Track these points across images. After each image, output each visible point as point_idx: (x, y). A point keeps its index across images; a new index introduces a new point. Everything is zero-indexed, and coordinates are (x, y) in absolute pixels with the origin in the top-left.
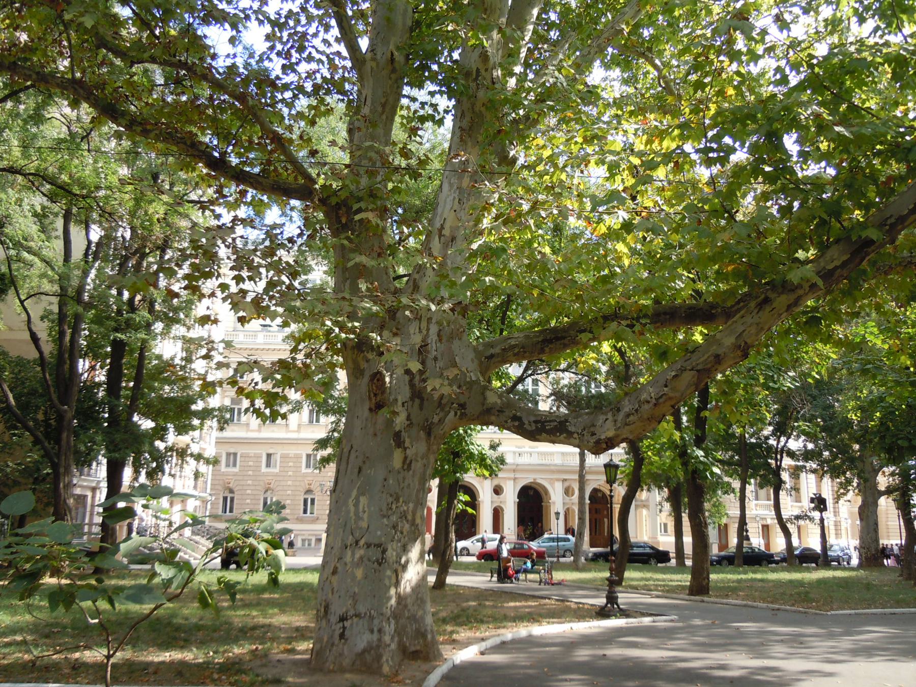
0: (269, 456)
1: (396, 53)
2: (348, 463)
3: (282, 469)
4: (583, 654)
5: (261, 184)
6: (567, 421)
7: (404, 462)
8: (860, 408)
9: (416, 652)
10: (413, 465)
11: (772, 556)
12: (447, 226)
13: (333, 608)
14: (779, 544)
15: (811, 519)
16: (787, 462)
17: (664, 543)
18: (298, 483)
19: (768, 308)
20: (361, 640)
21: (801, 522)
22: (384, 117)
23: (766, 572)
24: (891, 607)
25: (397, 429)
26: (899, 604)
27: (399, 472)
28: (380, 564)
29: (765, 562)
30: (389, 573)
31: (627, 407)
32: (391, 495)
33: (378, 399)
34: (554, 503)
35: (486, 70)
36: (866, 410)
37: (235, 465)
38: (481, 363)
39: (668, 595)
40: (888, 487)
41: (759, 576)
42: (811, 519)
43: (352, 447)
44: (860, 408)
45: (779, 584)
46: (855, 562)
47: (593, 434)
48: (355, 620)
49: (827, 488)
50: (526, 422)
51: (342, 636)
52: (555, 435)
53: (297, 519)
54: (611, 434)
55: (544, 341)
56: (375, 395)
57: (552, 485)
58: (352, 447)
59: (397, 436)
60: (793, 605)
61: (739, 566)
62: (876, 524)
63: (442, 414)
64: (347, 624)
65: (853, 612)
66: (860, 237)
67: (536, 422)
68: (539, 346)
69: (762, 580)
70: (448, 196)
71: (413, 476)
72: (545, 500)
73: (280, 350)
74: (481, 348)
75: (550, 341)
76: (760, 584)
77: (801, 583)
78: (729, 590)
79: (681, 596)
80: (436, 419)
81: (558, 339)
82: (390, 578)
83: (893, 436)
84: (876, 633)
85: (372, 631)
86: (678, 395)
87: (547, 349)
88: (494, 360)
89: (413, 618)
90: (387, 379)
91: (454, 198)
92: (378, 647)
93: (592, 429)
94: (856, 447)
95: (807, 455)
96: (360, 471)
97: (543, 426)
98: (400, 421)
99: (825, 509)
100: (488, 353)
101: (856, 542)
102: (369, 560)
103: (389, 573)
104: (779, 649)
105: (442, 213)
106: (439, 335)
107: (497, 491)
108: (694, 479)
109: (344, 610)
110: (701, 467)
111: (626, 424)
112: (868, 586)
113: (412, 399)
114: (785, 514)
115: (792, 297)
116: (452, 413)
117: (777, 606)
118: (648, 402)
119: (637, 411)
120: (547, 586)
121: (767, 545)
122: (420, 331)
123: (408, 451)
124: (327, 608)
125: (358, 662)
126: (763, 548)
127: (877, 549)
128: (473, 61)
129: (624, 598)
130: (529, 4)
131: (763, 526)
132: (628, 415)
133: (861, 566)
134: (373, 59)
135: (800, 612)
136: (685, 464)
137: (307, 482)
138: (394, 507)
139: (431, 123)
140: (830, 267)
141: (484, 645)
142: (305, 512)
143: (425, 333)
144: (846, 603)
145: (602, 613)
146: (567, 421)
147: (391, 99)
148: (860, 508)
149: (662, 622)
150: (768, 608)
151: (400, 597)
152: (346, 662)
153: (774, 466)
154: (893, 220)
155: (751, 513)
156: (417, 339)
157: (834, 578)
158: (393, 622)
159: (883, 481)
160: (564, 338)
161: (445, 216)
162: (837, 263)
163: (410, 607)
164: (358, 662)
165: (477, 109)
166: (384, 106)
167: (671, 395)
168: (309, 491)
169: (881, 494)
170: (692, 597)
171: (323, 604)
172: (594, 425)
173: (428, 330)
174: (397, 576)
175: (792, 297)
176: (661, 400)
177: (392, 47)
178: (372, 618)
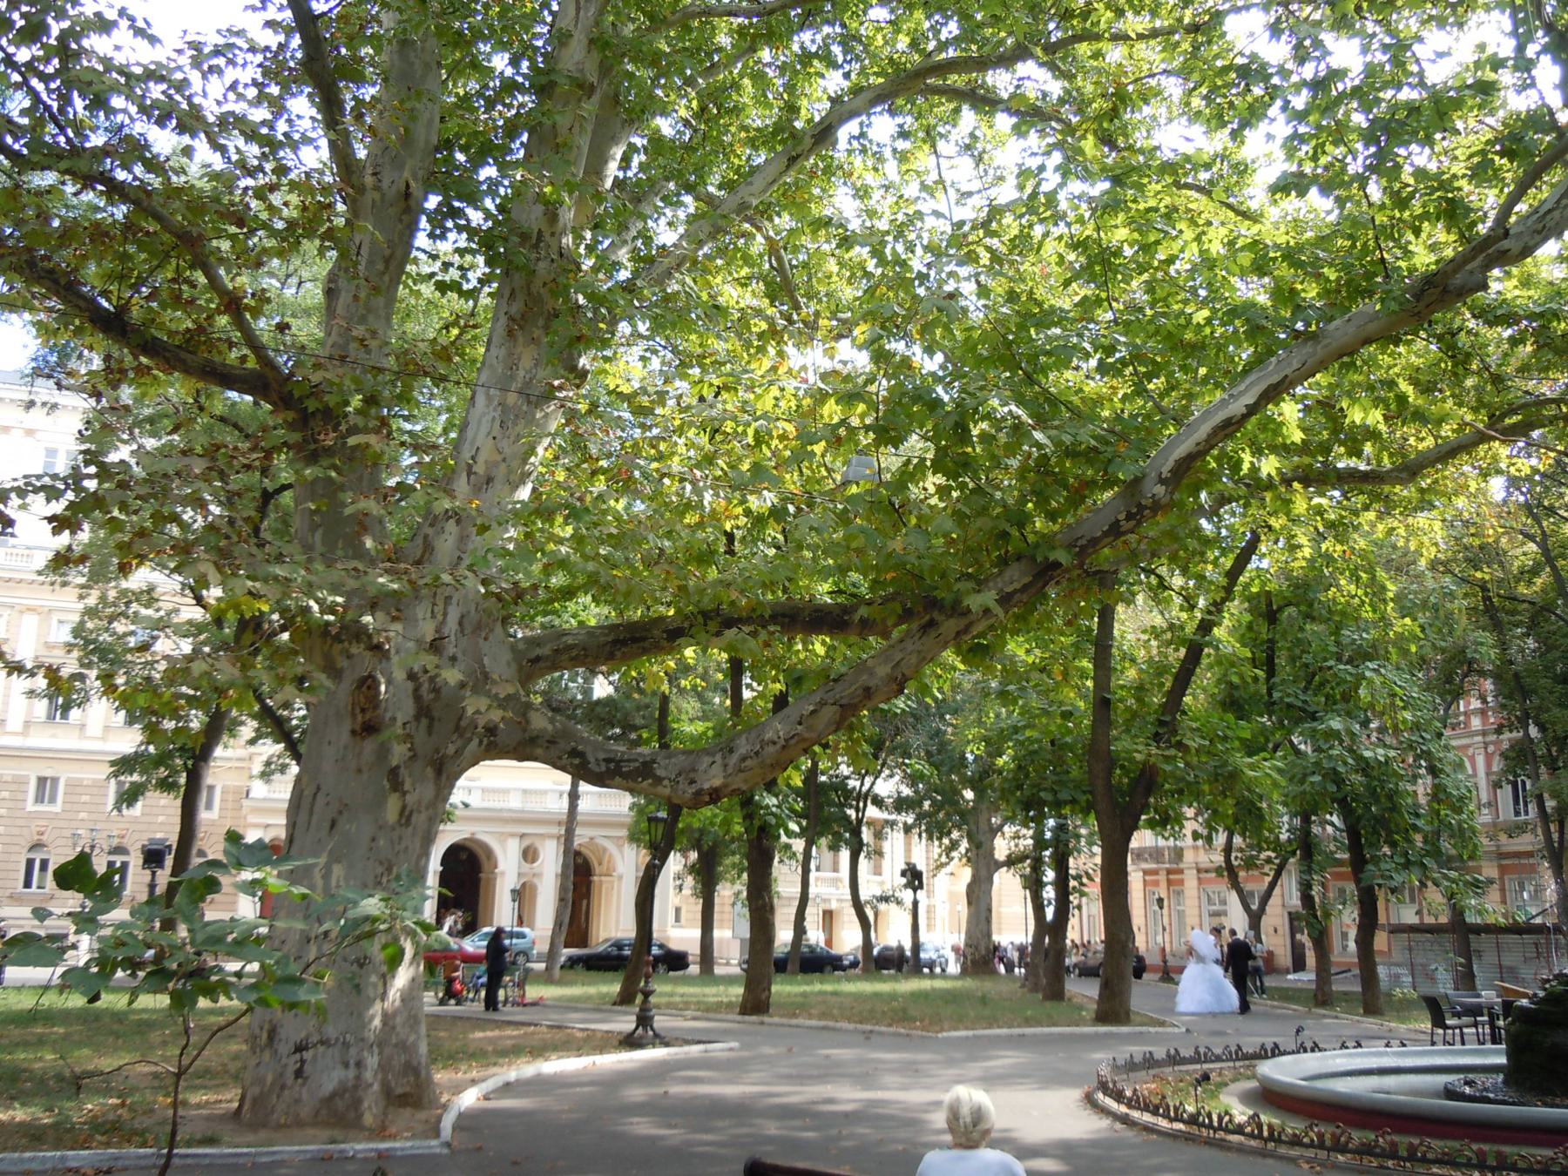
0: (42, 781)
1: (413, 184)
2: (311, 812)
3: (68, 807)
4: (637, 1094)
5: (184, 362)
6: (654, 761)
7: (401, 814)
8: (986, 740)
9: (405, 1095)
10: (414, 819)
11: (839, 958)
12: (481, 459)
13: (283, 1033)
14: (848, 940)
15: (899, 903)
16: (872, 812)
17: (682, 939)
18: (15, 831)
19: (933, 634)
20: (329, 1077)
21: (882, 907)
22: (386, 278)
23: (839, 980)
24: (1019, 1026)
25: (394, 763)
26: (1028, 1022)
27: (394, 829)
28: (361, 966)
29: (829, 968)
30: (374, 978)
31: (743, 747)
32: (381, 863)
33: (368, 717)
34: (503, 873)
35: (553, 234)
36: (994, 746)
37: (53, 800)
38: (520, 669)
39: (711, 1015)
40: (1009, 856)
41: (828, 987)
42: (899, 903)
43: (319, 789)
44: (986, 740)
45: (859, 997)
46: (954, 968)
47: (692, 782)
48: (321, 1049)
49: (923, 853)
50: (592, 760)
51: (299, 1073)
52: (635, 780)
53: (11, 897)
54: (717, 782)
55: (616, 642)
56: (363, 710)
57: (503, 842)
58: (319, 789)
59: (394, 773)
60: (890, 1025)
61: (793, 973)
62: (990, 911)
63: (459, 743)
64: (307, 1055)
65: (970, 1033)
66: (1047, 559)
67: (608, 761)
68: (608, 648)
69: (835, 994)
70: (484, 414)
71: (413, 835)
72: (485, 865)
73: (20, 581)
74: (521, 646)
75: (623, 643)
76: (833, 999)
77: (893, 996)
78: (799, 1007)
79: (730, 1017)
80: (451, 749)
81: (635, 640)
82: (375, 986)
83: (1033, 786)
84: (1007, 1059)
85: (346, 1065)
86: (813, 735)
87: (618, 654)
88: (542, 664)
89: (403, 1046)
90: (383, 688)
91: (494, 419)
92: (356, 1087)
93: (692, 775)
94: (969, 794)
95: (901, 804)
96: (333, 825)
97: (618, 767)
98: (399, 752)
99: (921, 886)
100: (533, 655)
101: (960, 939)
102: (345, 960)
103: (374, 978)
104: (890, 1079)
105: (474, 438)
106: (460, 624)
107: (529, 855)
108: (759, 838)
109: (303, 1035)
110: (773, 821)
111: (741, 771)
112: (984, 1000)
113: (417, 718)
114: (864, 895)
115: (963, 622)
116: (476, 741)
117: (869, 1027)
118: (774, 743)
119: (757, 753)
120: (516, 1009)
121: (829, 942)
122: (433, 616)
123: (408, 797)
124: (272, 1033)
125: (324, 1112)
126: (822, 944)
127: (987, 948)
128: (533, 217)
129: (660, 1022)
130: (613, 138)
131: (825, 912)
132: (744, 759)
133: (965, 971)
134: (377, 188)
135: (900, 1035)
136: (749, 817)
137: (35, 830)
138: (384, 880)
139: (455, 296)
140: (1009, 589)
141: (490, 1085)
142: (28, 884)
143: (440, 618)
144: (959, 1022)
145: (630, 1042)
146: (654, 761)
147: (399, 253)
148: (969, 886)
149: (718, 1049)
150: (856, 1031)
151: (386, 1017)
152: (305, 1112)
153: (854, 816)
154: (1084, 542)
155: (822, 894)
156: (428, 630)
157: (934, 990)
158: (376, 1049)
159: (1002, 847)
160: (644, 639)
161: (478, 444)
162: (1017, 586)
163: (398, 1029)
164: (324, 1112)
165: (534, 290)
166: (387, 261)
167: (806, 735)
168: (37, 846)
169: (999, 865)
170: (747, 1018)
171: (266, 1027)
172: (694, 770)
173: (445, 614)
174: (385, 984)
175: (963, 622)
176: (793, 742)
177: (406, 174)
178: (346, 1045)
